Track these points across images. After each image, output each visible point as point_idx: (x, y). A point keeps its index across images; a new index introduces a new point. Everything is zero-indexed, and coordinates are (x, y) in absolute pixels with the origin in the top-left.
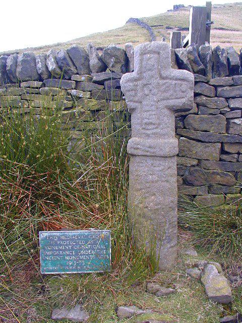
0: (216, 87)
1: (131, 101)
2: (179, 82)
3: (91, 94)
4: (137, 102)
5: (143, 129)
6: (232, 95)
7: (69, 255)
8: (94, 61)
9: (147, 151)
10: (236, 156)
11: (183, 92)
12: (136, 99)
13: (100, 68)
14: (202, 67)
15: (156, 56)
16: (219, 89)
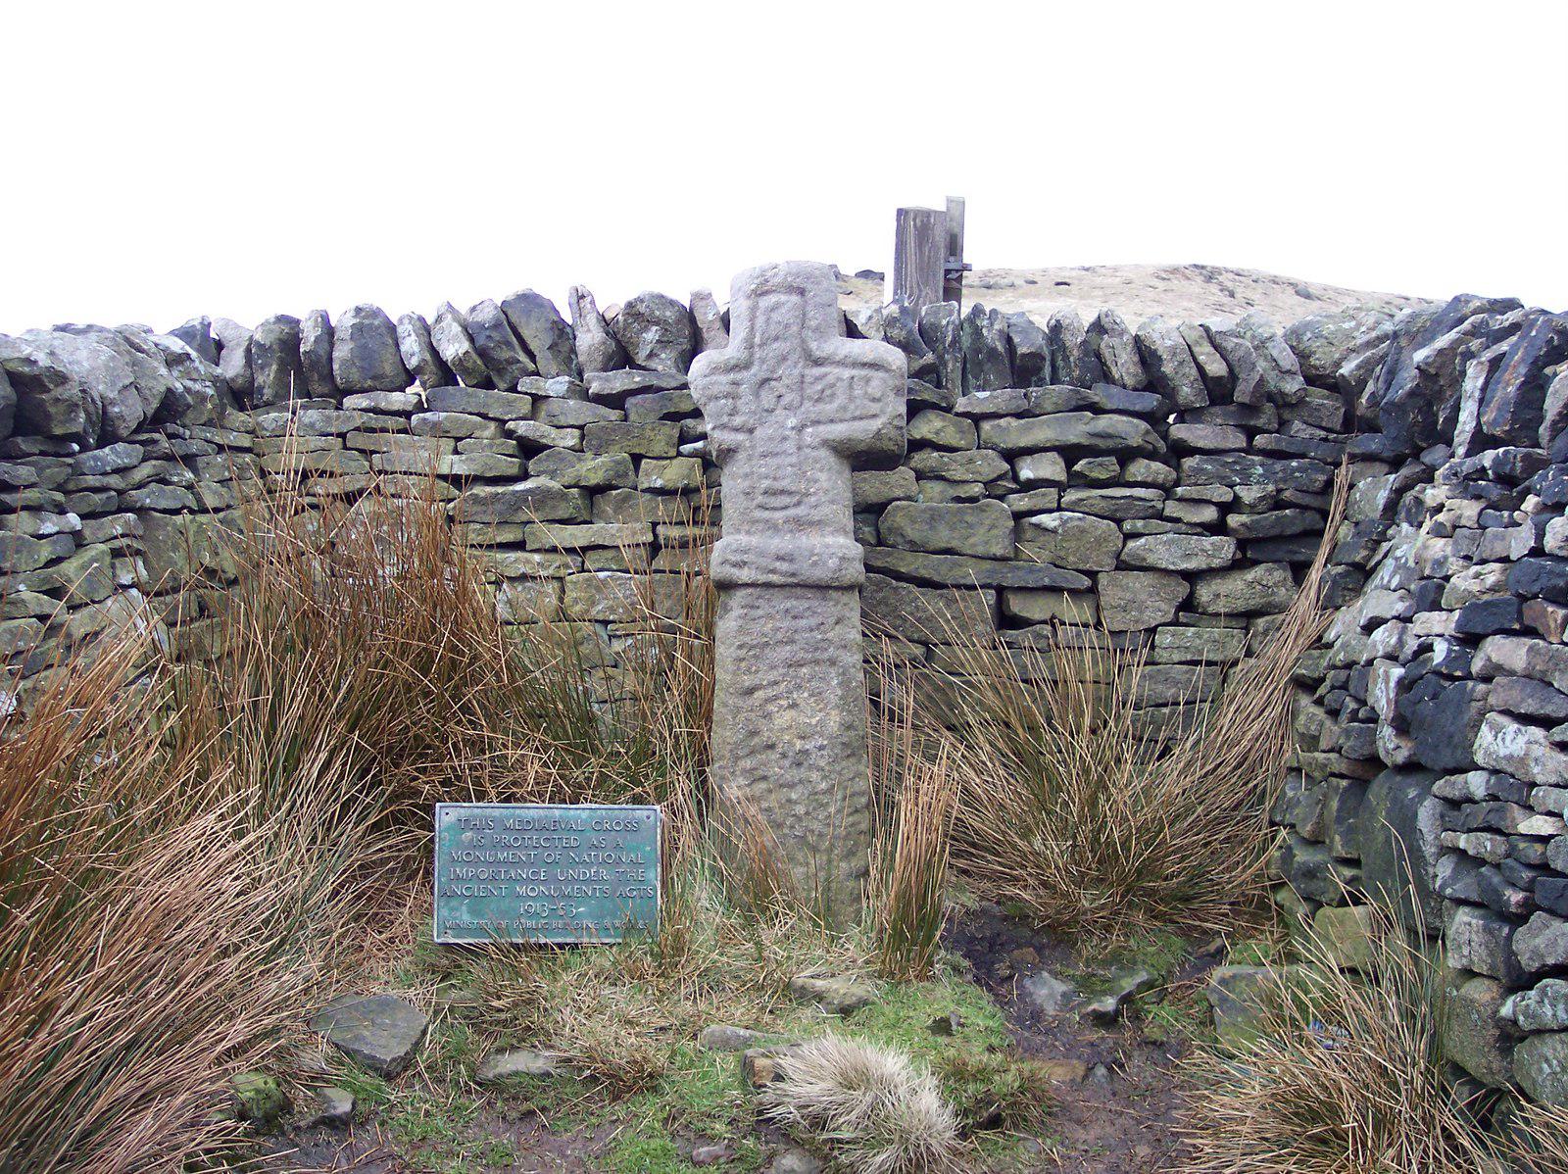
0: (977, 419)
1: (724, 427)
2: (864, 372)
3: (582, 437)
4: (737, 430)
5: (762, 507)
6: (1024, 442)
7: (528, 881)
8: (589, 339)
9: (773, 571)
10: (1047, 630)
11: (874, 400)
12: (738, 421)
13: (610, 358)
14: (929, 358)
15: (795, 298)
16: (986, 426)
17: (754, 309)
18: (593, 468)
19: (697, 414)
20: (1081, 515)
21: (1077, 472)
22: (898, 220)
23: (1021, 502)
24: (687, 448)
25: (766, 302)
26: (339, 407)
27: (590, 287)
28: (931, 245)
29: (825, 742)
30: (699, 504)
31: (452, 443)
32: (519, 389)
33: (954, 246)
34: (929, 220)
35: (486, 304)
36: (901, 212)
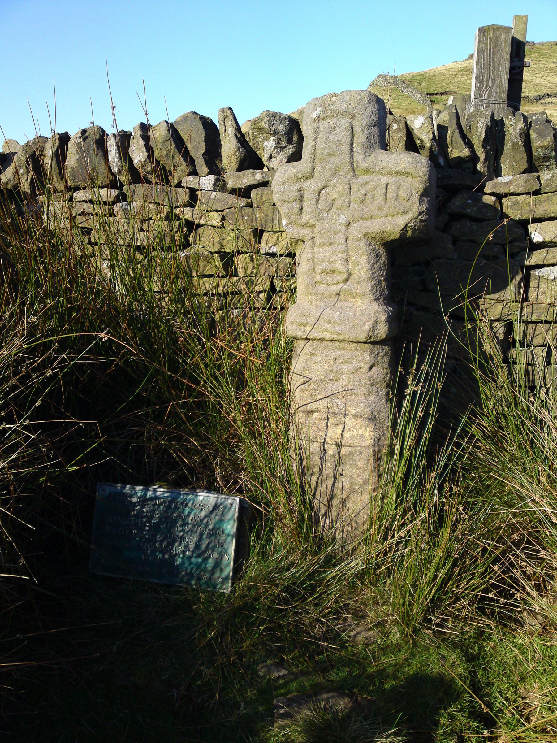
25: (323, 125)
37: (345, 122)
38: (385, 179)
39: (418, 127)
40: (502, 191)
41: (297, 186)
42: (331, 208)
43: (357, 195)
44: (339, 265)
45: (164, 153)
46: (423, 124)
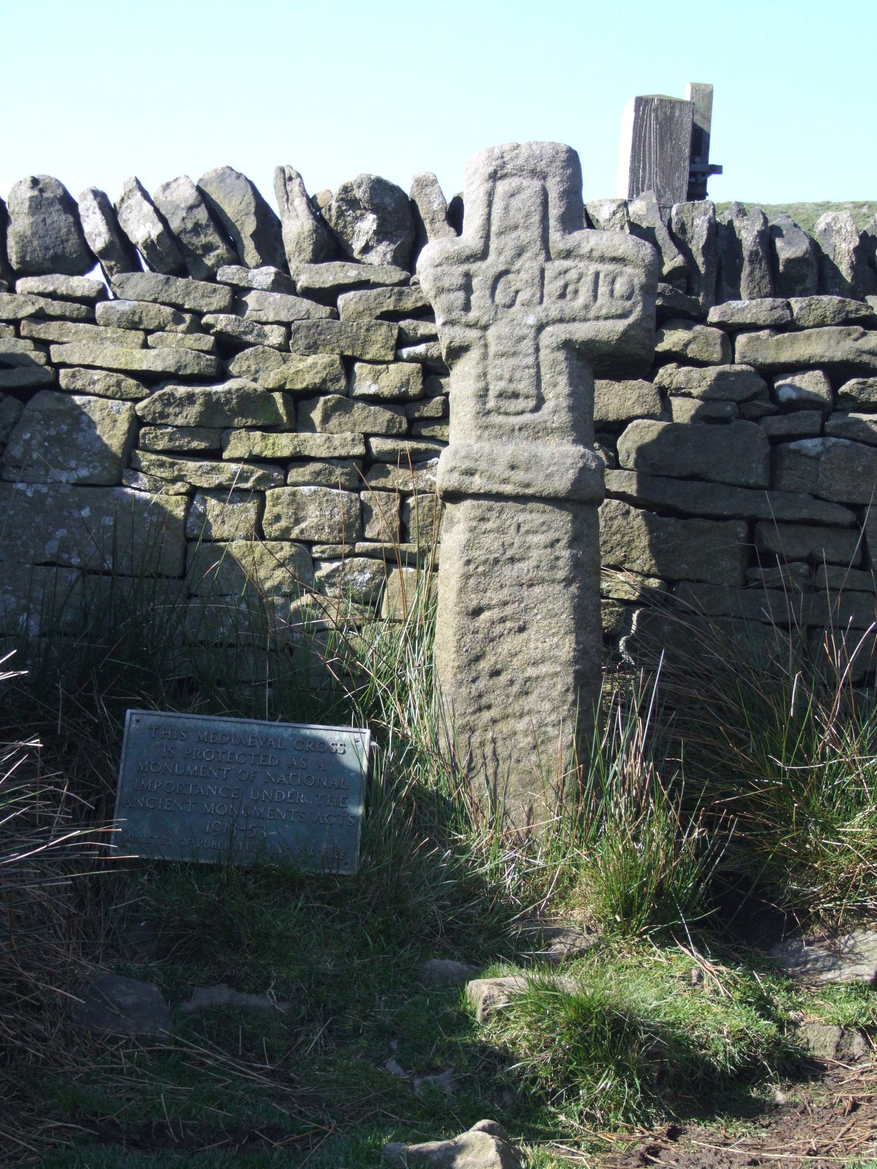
4: (469, 326)
6: (786, 356)
17: (491, 194)
18: (308, 368)
19: (425, 313)
20: (847, 442)
21: (846, 395)
22: (637, 110)
23: (779, 425)
24: (405, 352)
25: (502, 187)
26: (12, 290)
27: (298, 168)
28: (677, 142)
29: (558, 669)
30: (418, 414)
31: (141, 335)
32: (218, 278)
33: (700, 140)
34: (673, 113)
35: (181, 181)
36: (642, 103)
37: (536, 184)
38: (593, 267)
39: (607, 217)
40: (738, 319)
41: (465, 267)
42: (511, 305)
43: (552, 288)
44: (524, 386)
45: (190, 226)
46: (614, 213)
